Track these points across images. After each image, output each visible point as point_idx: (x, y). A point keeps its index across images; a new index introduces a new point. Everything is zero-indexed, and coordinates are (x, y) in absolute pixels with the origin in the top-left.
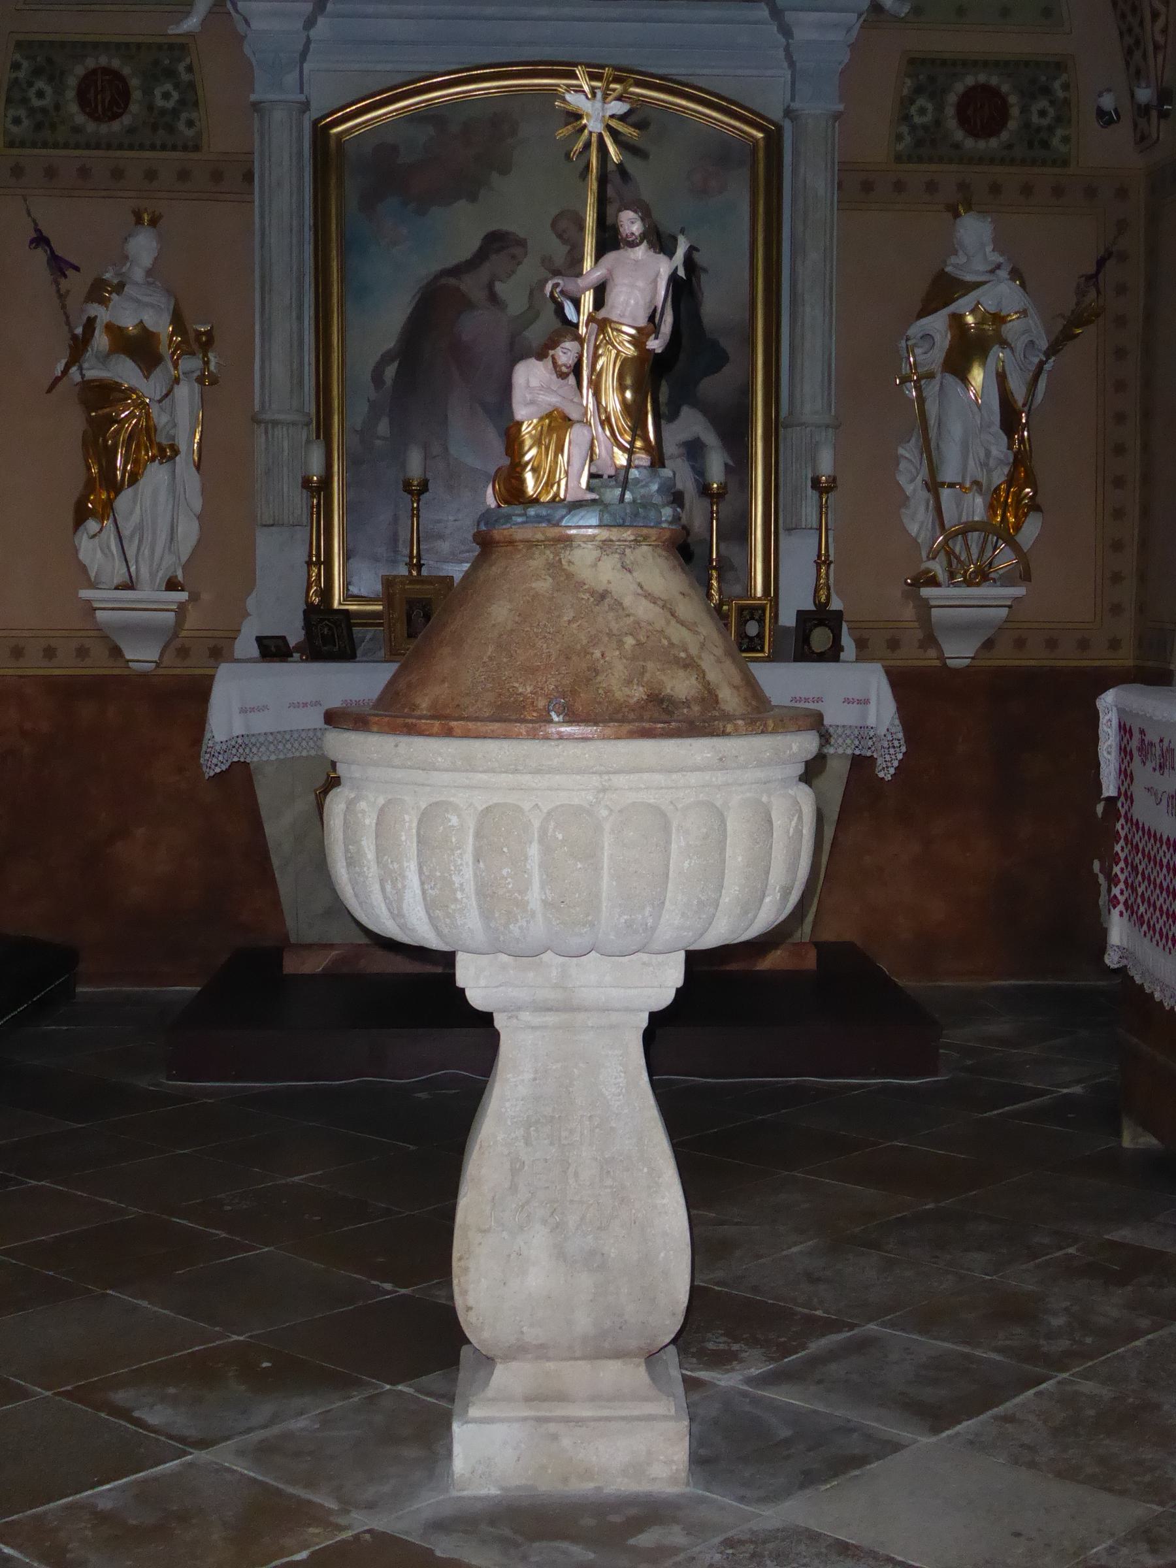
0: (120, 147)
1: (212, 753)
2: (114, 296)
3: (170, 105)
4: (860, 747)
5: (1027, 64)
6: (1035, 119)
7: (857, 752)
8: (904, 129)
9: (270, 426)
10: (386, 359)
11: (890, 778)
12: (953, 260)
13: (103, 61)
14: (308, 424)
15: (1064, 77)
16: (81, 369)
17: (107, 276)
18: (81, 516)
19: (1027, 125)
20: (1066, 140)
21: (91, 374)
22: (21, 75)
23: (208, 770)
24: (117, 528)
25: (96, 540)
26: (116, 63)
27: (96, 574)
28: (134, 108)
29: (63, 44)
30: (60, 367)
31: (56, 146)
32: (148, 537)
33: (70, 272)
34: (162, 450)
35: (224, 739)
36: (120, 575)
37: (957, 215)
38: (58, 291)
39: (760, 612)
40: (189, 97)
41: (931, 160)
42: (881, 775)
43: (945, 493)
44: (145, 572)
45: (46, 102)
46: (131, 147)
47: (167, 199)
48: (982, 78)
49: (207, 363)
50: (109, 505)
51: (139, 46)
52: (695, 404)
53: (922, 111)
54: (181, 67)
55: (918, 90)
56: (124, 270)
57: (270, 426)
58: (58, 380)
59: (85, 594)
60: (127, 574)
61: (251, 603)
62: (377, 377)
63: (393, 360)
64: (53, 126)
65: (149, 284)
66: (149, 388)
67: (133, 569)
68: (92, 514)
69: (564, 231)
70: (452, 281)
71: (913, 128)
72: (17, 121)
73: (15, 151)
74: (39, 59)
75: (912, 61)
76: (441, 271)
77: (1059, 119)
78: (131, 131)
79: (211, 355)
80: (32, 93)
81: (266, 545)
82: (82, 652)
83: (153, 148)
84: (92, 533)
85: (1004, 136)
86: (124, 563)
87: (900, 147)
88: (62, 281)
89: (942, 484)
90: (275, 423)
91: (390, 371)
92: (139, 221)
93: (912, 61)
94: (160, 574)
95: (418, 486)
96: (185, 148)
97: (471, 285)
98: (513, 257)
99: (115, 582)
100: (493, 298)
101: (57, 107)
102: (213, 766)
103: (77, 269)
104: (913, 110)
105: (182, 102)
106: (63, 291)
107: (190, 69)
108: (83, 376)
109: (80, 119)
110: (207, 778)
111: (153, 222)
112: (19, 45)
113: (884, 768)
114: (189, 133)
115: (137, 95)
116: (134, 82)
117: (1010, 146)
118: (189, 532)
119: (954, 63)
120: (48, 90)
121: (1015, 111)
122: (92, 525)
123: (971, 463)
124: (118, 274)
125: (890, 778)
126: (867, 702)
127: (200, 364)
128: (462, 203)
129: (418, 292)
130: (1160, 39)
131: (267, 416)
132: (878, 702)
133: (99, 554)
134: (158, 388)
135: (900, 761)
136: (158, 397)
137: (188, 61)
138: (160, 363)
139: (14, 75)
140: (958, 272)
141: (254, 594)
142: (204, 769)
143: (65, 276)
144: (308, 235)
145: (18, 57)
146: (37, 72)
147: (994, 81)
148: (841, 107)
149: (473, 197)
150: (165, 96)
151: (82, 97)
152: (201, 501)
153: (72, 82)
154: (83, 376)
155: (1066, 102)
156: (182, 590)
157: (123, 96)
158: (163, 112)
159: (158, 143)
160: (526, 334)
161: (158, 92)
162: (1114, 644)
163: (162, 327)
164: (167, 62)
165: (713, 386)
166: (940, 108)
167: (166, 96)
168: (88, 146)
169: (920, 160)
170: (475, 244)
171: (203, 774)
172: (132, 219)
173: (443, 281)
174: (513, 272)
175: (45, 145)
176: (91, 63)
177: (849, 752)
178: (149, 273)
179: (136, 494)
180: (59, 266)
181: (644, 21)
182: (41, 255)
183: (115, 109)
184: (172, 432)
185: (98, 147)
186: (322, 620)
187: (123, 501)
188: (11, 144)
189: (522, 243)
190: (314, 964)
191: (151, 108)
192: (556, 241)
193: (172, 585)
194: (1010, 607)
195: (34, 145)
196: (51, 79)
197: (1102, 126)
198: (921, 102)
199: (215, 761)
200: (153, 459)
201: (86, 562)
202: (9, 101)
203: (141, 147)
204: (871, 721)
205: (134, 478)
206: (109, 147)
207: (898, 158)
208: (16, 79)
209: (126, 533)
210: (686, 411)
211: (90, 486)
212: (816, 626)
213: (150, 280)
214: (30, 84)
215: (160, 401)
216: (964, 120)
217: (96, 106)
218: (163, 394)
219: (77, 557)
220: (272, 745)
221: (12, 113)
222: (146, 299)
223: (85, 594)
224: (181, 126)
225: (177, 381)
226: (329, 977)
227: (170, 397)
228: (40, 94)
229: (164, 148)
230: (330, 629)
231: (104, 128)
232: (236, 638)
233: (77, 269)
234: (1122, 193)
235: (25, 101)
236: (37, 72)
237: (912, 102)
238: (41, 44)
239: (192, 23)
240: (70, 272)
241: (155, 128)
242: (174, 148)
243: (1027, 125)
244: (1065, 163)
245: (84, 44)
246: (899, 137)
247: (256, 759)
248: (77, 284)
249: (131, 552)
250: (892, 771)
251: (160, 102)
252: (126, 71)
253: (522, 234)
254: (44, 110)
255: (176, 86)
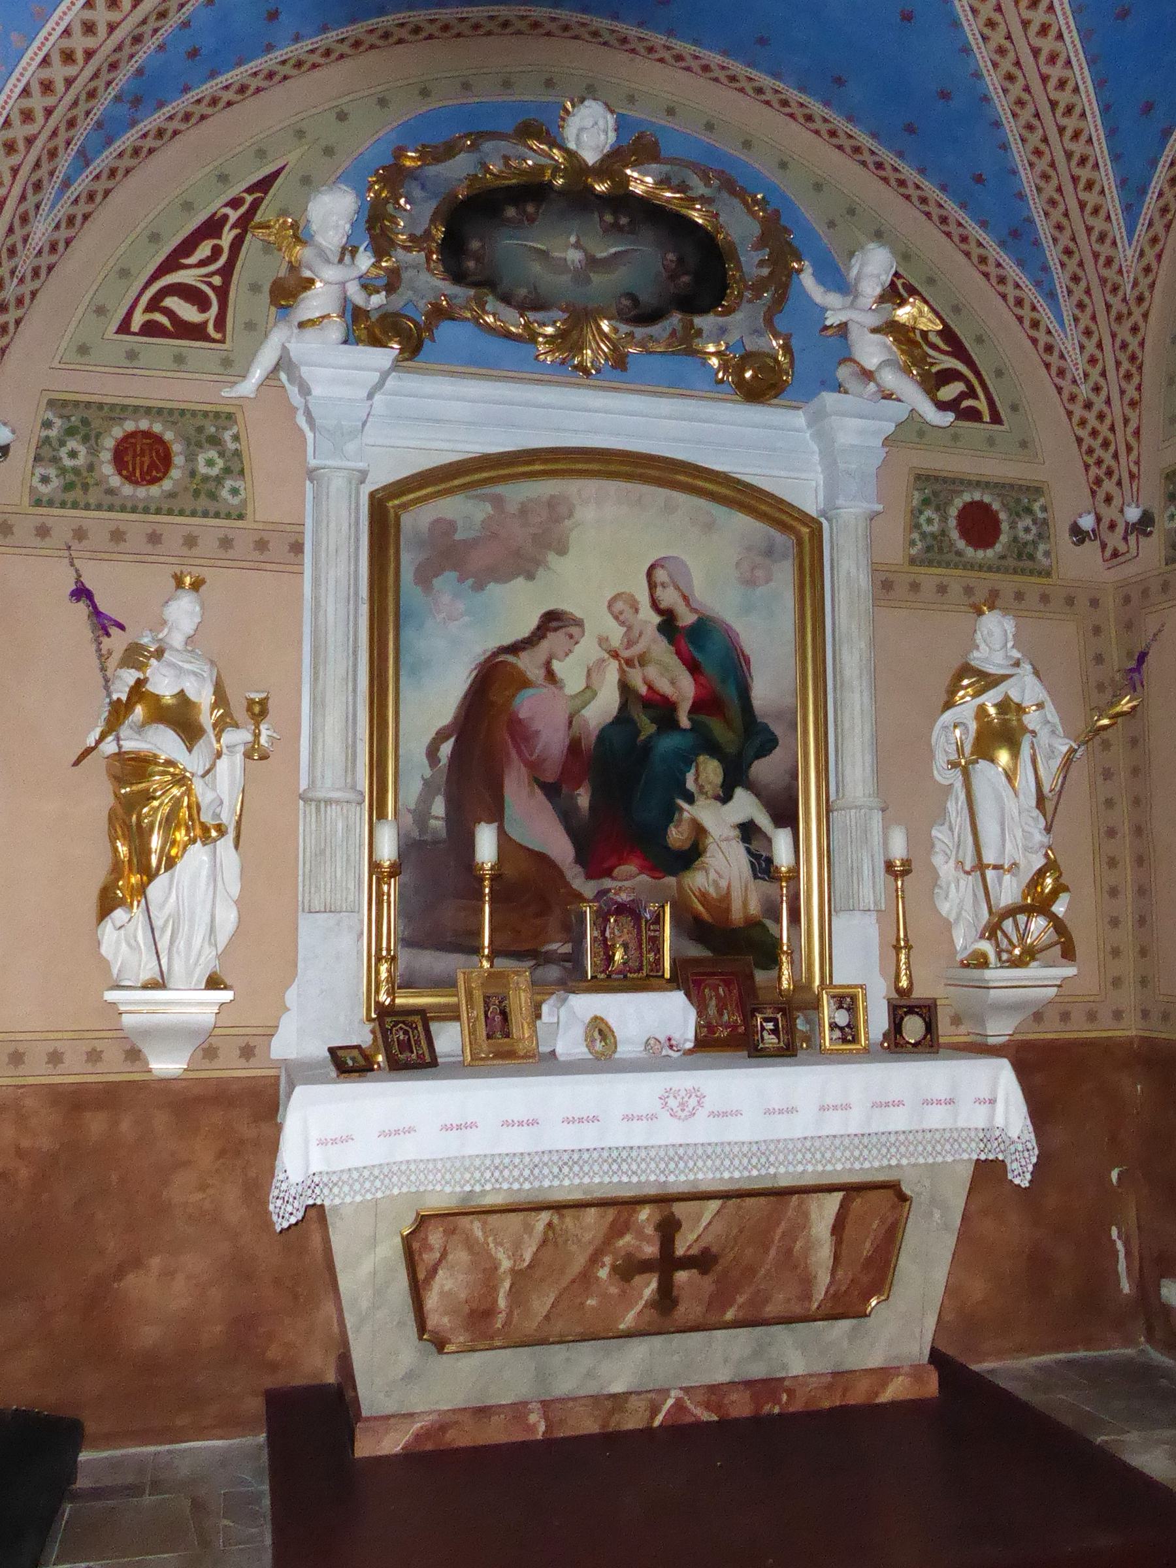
0: (158, 512)
1: (286, 1199)
2: (153, 661)
3: (214, 471)
4: (986, 1151)
5: (1012, 486)
6: (1021, 534)
7: (983, 1157)
8: (916, 536)
9: (323, 805)
10: (441, 736)
11: (1027, 1185)
12: (976, 654)
13: (144, 425)
14: (360, 803)
15: (1042, 501)
16: (118, 739)
17: (145, 641)
18: (107, 904)
19: (1015, 539)
20: (1047, 554)
21: (129, 745)
22: (53, 433)
23: (280, 1220)
24: (149, 917)
25: (122, 931)
26: (157, 428)
27: (119, 971)
28: (175, 473)
29: (101, 406)
30: (95, 734)
31: (87, 507)
32: (185, 928)
33: (113, 630)
34: (205, 829)
35: (300, 1180)
36: (148, 971)
37: (980, 613)
38: (99, 650)
39: (848, 1000)
40: (235, 467)
41: (939, 565)
42: (1017, 1181)
43: (990, 874)
44: (178, 967)
45: (81, 461)
46: (170, 512)
47: (565, 430)
48: (977, 496)
49: (257, 736)
50: (142, 890)
51: (183, 412)
52: (750, 787)
53: (929, 521)
54: (227, 436)
55: (926, 502)
56: (161, 636)
57: (323, 805)
58: (89, 751)
59: (111, 996)
60: (157, 968)
61: (291, 996)
62: (432, 753)
63: (447, 738)
64: (85, 487)
65: (187, 651)
66: (191, 761)
67: (164, 961)
68: (121, 903)
69: (621, 613)
70: (510, 658)
71: (923, 535)
72: (45, 480)
73: (41, 510)
74: (73, 419)
75: (918, 477)
76: (499, 648)
77: (1040, 536)
78: (172, 495)
79: (263, 727)
80: (63, 453)
81: (310, 930)
82: (94, 1056)
83: (193, 514)
84: (118, 924)
85: (998, 547)
86: (155, 956)
87: (913, 551)
88: (105, 640)
89: (988, 866)
90: (328, 802)
91: (446, 749)
92: (179, 584)
93: (918, 477)
94: (198, 970)
95: (491, 869)
96: (228, 516)
97: (529, 664)
98: (571, 636)
99: (142, 977)
100: (551, 676)
101: (91, 468)
102: (287, 1215)
103: (122, 627)
104: (922, 519)
105: (227, 471)
106: (104, 652)
107: (236, 438)
108: (120, 747)
109: (115, 481)
110: (279, 1230)
111: (196, 586)
112: (51, 403)
113: (1019, 1175)
114: (235, 501)
115: (179, 460)
116: (176, 448)
117: (1003, 557)
118: (228, 918)
119: (954, 481)
120: (82, 450)
121: (1005, 526)
122: (119, 915)
123: (1008, 845)
124: (155, 640)
125: (1027, 1185)
126: (992, 1101)
127: (249, 737)
128: (520, 581)
129: (475, 668)
130: (1135, 469)
131: (320, 794)
132: (1007, 1102)
133: (124, 946)
134: (201, 762)
135: (1035, 1165)
136: (201, 772)
137: (235, 430)
138: (202, 735)
139: (44, 433)
140: (983, 664)
141: (294, 986)
142: (275, 1218)
143: (108, 635)
144: (364, 609)
145: (49, 415)
146: (71, 432)
147: (987, 499)
148: (879, 507)
149: (530, 576)
150: (208, 462)
151: (119, 459)
152: (240, 886)
153: (109, 443)
154: (120, 747)
155: (1045, 522)
156: (226, 988)
157: (165, 461)
158: (206, 479)
159: (199, 509)
160: (583, 712)
161: (201, 460)
162: (1118, 1015)
163: (202, 696)
164: (213, 429)
165: (763, 769)
166: (944, 519)
167: (210, 463)
168: (123, 509)
169: (930, 563)
170: (533, 622)
171: (273, 1224)
172: (173, 583)
173: (501, 658)
174: (571, 651)
175: (75, 505)
176: (130, 426)
177: (975, 1157)
178: (189, 640)
179: (172, 877)
180: (102, 623)
181: (691, 420)
182: (82, 608)
183: (154, 473)
184: (218, 810)
185: (134, 510)
186: (397, 1023)
187: (155, 890)
188: (38, 503)
189: (579, 623)
190: (392, 1443)
191: (193, 474)
192: (613, 623)
193: (213, 983)
194: (1059, 986)
195: (63, 505)
196: (86, 439)
197: (1075, 544)
198: (928, 513)
199: (289, 1209)
200: (193, 841)
201: (110, 957)
202: (37, 459)
203: (181, 513)
204: (999, 1121)
205: (171, 863)
206: (146, 510)
207: (913, 561)
208: (47, 437)
209: (158, 923)
210: (740, 794)
211: (117, 869)
212: (906, 1013)
213: (189, 648)
214: (62, 443)
215: (203, 776)
216: (965, 533)
217: (134, 469)
218: (207, 768)
219: (99, 953)
220: (357, 1184)
221: (40, 471)
222: (186, 666)
223: (111, 996)
224: (225, 493)
225: (219, 755)
226: (410, 1459)
227: (213, 772)
228: (73, 454)
229: (205, 514)
230: (406, 1033)
231: (142, 492)
232: (273, 1035)
233: (122, 627)
234: (1094, 603)
235: (55, 460)
236: (71, 432)
237: (921, 512)
238: (76, 404)
239: (248, 386)
240: (113, 630)
241: (197, 494)
242: (217, 515)
243: (1015, 539)
244: (1048, 574)
245: (124, 408)
246: (913, 543)
247: (337, 1201)
248: (117, 642)
249: (163, 944)
250: (1028, 1177)
251: (203, 469)
252: (168, 436)
253: (578, 614)
254: (76, 471)
255: (221, 454)
